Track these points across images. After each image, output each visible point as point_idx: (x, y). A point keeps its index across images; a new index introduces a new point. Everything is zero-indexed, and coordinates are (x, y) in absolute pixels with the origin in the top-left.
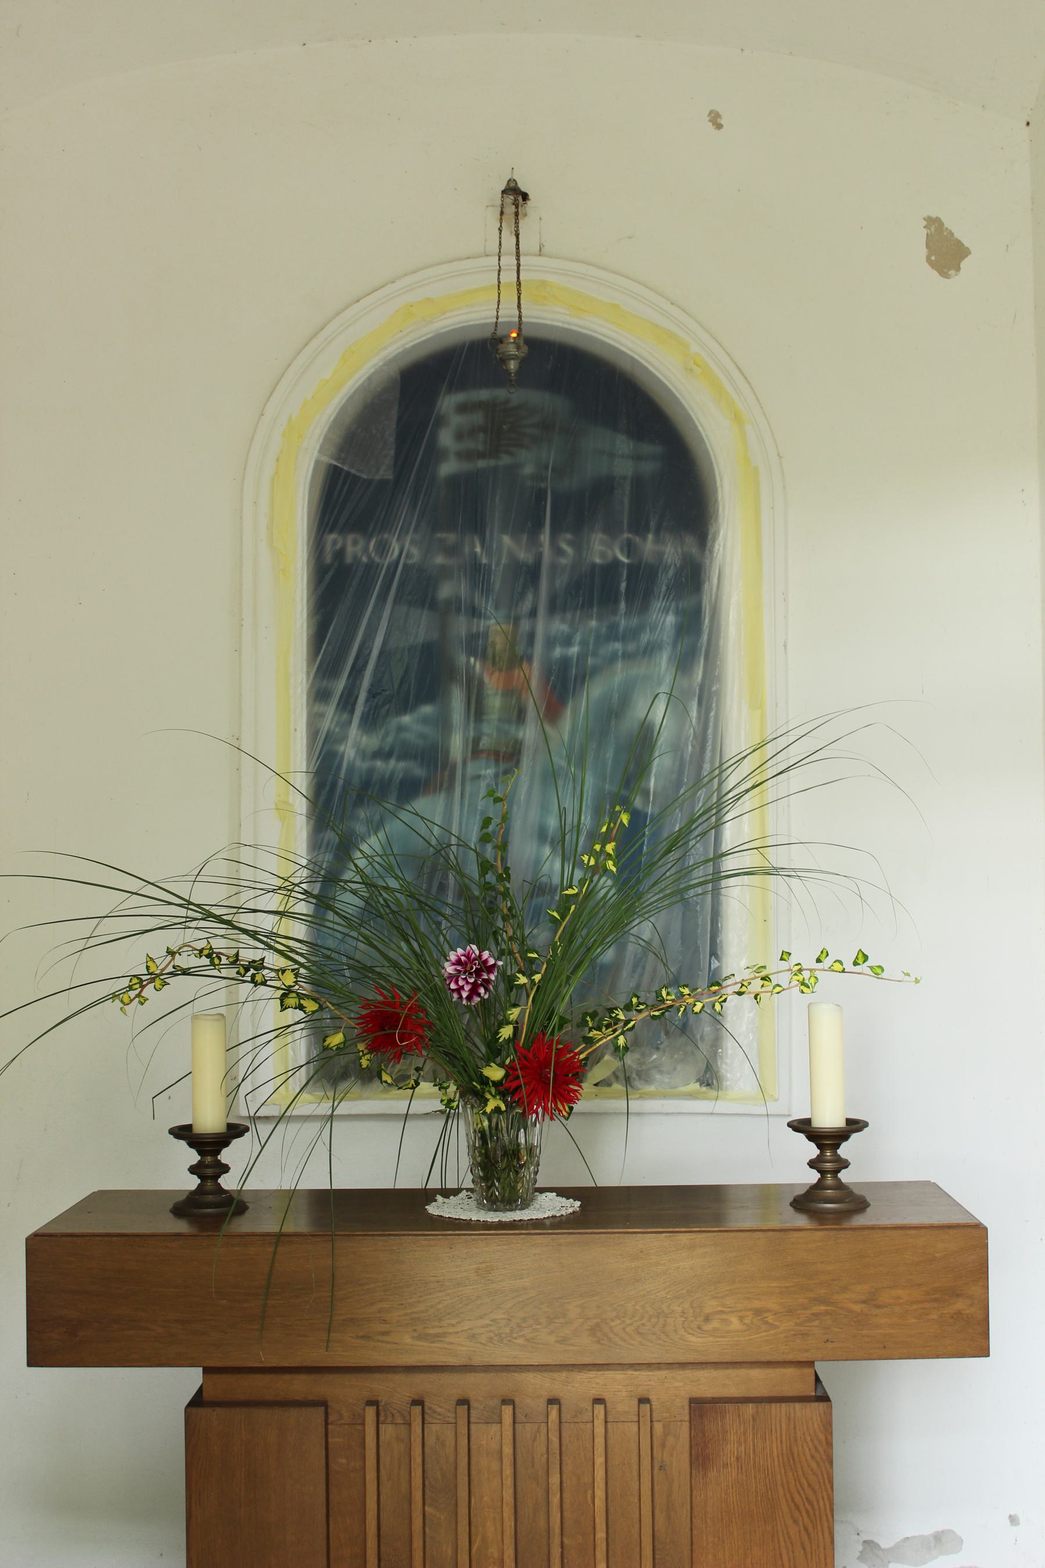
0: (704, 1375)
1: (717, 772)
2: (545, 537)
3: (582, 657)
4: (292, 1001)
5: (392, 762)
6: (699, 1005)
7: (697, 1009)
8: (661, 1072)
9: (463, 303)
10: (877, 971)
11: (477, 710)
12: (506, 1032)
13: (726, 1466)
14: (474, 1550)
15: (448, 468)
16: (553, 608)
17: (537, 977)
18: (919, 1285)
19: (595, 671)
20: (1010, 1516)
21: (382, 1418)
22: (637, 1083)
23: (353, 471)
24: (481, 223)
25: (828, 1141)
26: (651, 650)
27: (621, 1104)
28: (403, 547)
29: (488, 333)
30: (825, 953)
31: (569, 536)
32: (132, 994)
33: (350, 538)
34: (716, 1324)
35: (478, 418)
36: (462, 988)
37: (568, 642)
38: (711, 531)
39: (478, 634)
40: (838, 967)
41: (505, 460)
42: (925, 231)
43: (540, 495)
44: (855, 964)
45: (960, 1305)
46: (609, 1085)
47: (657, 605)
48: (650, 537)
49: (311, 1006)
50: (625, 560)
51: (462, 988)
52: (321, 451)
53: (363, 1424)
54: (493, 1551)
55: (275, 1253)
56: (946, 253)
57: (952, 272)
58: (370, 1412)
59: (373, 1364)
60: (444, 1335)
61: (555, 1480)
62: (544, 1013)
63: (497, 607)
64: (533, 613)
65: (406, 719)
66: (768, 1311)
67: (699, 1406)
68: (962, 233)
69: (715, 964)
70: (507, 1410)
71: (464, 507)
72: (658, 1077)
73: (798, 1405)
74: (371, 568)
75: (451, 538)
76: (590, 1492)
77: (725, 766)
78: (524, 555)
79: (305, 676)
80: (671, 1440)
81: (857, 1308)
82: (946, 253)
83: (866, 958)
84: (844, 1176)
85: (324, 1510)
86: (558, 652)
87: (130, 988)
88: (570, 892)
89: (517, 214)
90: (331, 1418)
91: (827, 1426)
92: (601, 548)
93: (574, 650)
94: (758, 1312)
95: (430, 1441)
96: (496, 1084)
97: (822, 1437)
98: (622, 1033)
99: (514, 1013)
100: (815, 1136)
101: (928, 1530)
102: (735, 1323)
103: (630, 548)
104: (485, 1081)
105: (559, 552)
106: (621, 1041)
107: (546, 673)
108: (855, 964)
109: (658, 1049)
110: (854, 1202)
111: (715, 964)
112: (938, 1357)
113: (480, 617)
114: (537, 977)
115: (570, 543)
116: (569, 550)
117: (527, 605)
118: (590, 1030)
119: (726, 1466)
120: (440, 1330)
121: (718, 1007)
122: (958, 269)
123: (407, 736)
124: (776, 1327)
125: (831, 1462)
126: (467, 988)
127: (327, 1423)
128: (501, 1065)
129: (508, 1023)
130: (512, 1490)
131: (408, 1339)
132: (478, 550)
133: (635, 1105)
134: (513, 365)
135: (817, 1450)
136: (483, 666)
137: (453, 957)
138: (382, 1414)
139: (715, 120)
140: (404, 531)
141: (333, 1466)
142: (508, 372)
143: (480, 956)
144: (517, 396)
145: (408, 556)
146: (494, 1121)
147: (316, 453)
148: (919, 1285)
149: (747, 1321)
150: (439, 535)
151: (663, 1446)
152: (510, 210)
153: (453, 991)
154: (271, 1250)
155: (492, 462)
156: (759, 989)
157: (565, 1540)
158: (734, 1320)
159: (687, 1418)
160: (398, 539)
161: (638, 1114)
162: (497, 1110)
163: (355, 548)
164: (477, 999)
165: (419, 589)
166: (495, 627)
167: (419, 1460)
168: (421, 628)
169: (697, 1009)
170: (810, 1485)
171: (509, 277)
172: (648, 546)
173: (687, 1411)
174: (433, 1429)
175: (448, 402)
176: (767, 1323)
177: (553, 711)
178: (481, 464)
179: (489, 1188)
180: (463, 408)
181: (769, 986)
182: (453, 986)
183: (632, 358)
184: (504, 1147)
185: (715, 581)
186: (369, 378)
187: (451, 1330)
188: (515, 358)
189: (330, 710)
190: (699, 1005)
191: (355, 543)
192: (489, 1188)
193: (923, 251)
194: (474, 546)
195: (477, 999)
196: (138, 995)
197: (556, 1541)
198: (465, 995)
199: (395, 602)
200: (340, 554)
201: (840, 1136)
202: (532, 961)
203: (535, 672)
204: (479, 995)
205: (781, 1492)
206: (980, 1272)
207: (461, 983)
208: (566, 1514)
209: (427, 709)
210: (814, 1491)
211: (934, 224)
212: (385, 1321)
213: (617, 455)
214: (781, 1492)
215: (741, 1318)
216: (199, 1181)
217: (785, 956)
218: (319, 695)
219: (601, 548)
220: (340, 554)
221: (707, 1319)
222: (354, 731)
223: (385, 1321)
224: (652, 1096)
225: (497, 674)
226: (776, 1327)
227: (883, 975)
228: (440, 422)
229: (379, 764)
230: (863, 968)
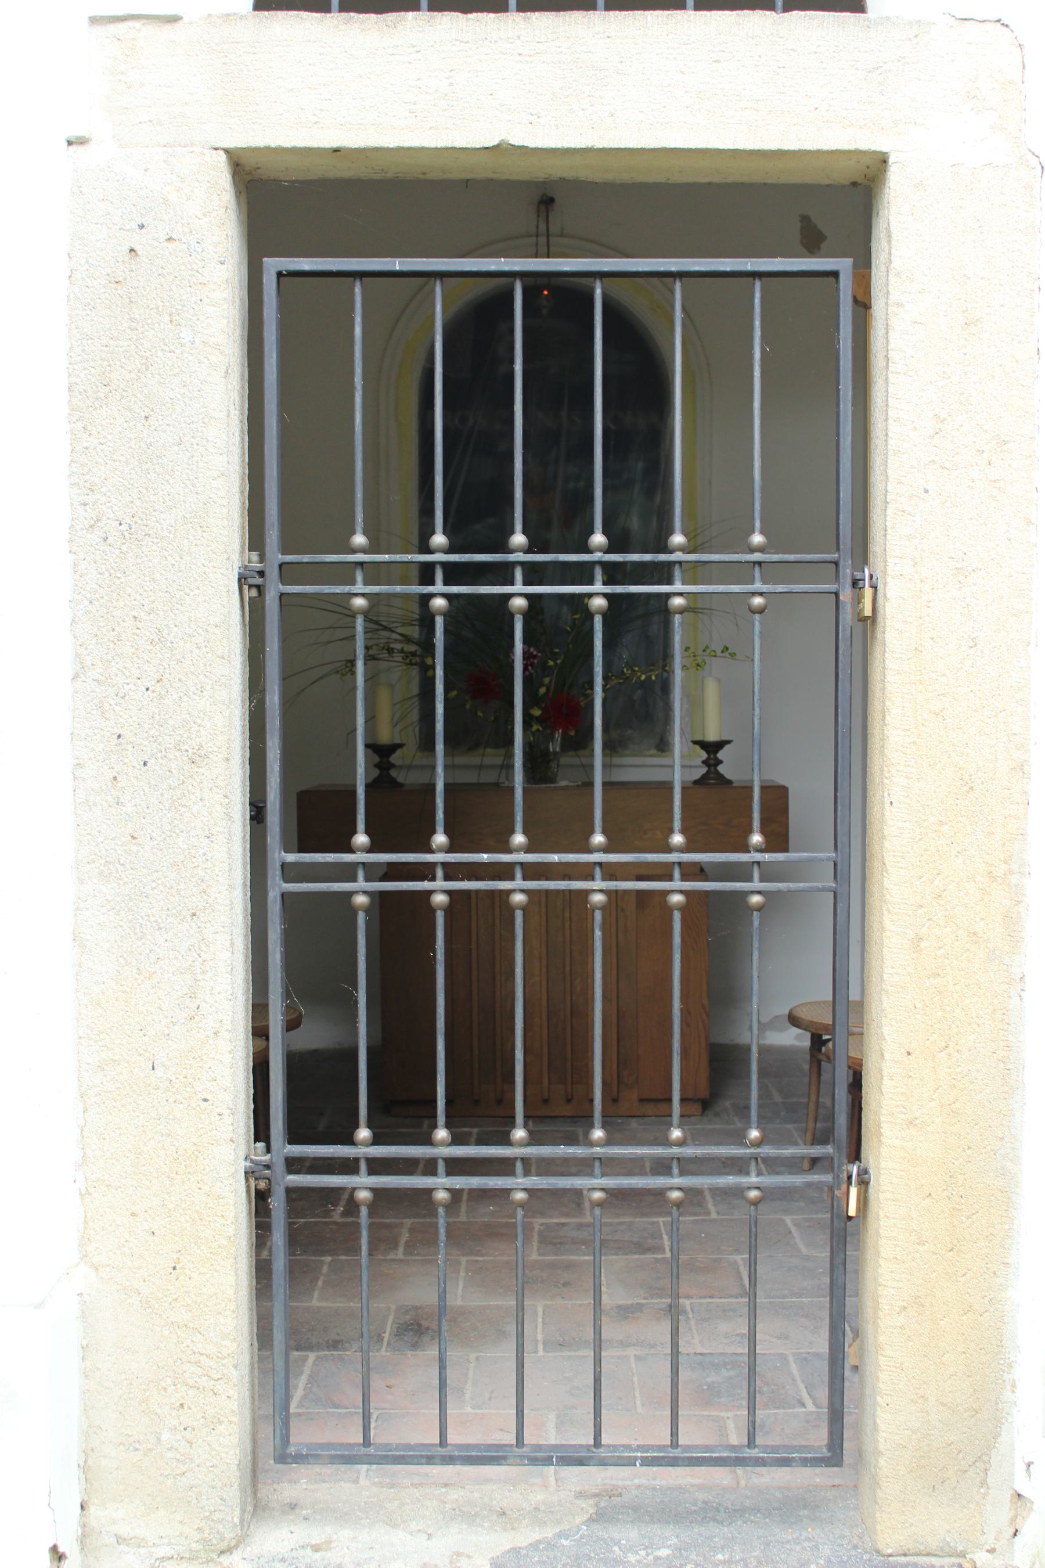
10: (733, 655)
17: (559, 661)
25: (712, 748)
30: (707, 647)
61: (567, 915)
65: (478, 527)
83: (727, 649)
84: (720, 768)
86: (571, 485)
96: (537, 718)
99: (547, 680)
110: (724, 782)
114: (559, 661)
122: (819, 249)
128: (540, 708)
134: (545, 311)
158: (659, 833)
162: (538, 730)
201: (720, 745)
202: (556, 653)
211: (806, 220)
230: (726, 654)
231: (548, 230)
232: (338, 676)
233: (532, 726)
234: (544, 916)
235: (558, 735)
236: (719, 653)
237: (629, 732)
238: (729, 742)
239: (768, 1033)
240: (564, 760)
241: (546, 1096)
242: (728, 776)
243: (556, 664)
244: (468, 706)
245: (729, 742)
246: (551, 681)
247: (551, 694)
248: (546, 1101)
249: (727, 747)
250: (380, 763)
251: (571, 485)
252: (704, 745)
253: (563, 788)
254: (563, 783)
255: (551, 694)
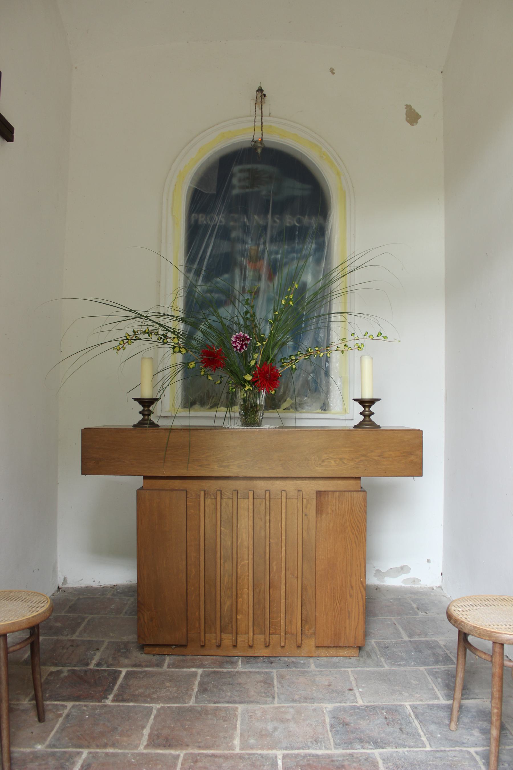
0: (322, 482)
1: (329, 295)
2: (269, 216)
3: (282, 259)
4: (177, 349)
5: (213, 294)
6: (322, 354)
7: (321, 355)
8: (307, 406)
9: (240, 132)
11: (244, 278)
12: (253, 363)
13: (329, 513)
14: (238, 543)
15: (235, 192)
16: (272, 241)
17: (264, 343)
18: (399, 450)
19: (286, 264)
20: (428, 560)
21: (206, 496)
22: (299, 409)
23: (202, 190)
24: (248, 104)
25: (367, 404)
26: (306, 257)
27: (293, 415)
28: (219, 219)
29: (249, 145)
31: (277, 216)
32: (121, 346)
33: (200, 215)
34: (326, 463)
35: (246, 175)
36: (238, 346)
37: (277, 253)
38: (329, 213)
39: (245, 250)
40: (371, 337)
41: (256, 189)
42: (405, 110)
43: (268, 201)
44: (378, 336)
45: (412, 458)
46: (289, 410)
47: (308, 240)
48: (306, 217)
49: (183, 351)
50: (298, 225)
51: (238, 346)
52: (191, 183)
53: (200, 498)
54: (245, 544)
55: (169, 435)
56: (413, 117)
57: (414, 124)
58: (202, 493)
59: (203, 476)
60: (229, 465)
61: (268, 518)
62: (266, 358)
63: (252, 241)
64: (264, 243)
65: (218, 280)
66: (345, 459)
67: (319, 494)
68: (418, 110)
69: (327, 365)
70: (251, 494)
71: (241, 205)
72: (306, 407)
73: (354, 493)
74: (207, 227)
75: (236, 216)
76: (280, 524)
77: (332, 294)
78: (261, 223)
79: (183, 261)
80: (309, 505)
81: (376, 458)
82: (413, 117)
83: (381, 334)
84: (372, 417)
85: (185, 527)
86: (273, 257)
87: (120, 344)
88: (277, 313)
89: (262, 102)
90: (188, 496)
91: (365, 500)
92: (289, 220)
93: (279, 256)
94: (341, 459)
95: (224, 504)
96: (249, 382)
97: (363, 504)
98: (294, 364)
99: (256, 356)
100: (362, 402)
101: (398, 565)
102: (333, 463)
103: (299, 221)
104: (245, 381)
105: (274, 222)
106: (294, 367)
107: (269, 265)
108: (378, 336)
109: (306, 396)
111: (327, 365)
112: (405, 476)
113: (246, 244)
114: (264, 343)
115: (278, 218)
116: (278, 221)
117: (262, 241)
118: (283, 363)
119: (329, 513)
120: (228, 464)
121: (328, 355)
122: (417, 123)
123: (218, 285)
124: (348, 464)
125: (366, 513)
126: (239, 346)
127: (187, 498)
129: (253, 359)
130: (252, 521)
131: (216, 467)
132: (246, 220)
133: (298, 415)
135: (361, 509)
136: (246, 261)
137: (234, 336)
138: (206, 495)
139: (332, 71)
140: (218, 214)
141: (189, 513)
142: (257, 153)
143: (244, 335)
144: (259, 167)
145: (221, 222)
146: (248, 393)
147: (189, 184)
148: (399, 450)
149: (337, 462)
150: (232, 215)
151: (306, 507)
152: (259, 100)
153: (234, 347)
154: (168, 434)
155: (251, 190)
156: (343, 349)
157: (271, 540)
158: (333, 462)
159: (315, 498)
160: (217, 215)
161: (299, 418)
162: (249, 389)
163: (202, 219)
164: (243, 350)
165: (224, 233)
166: (250, 246)
167: (219, 510)
168: (225, 247)
169: (321, 355)
170: (358, 521)
171: (259, 124)
172: (306, 220)
173: (315, 495)
174: (224, 500)
175: (236, 169)
176: (344, 463)
177: (271, 278)
178: (247, 190)
179: (246, 418)
180: (241, 171)
181: (347, 348)
182: (234, 345)
183: (302, 153)
184: (251, 404)
185: (330, 231)
186: (208, 158)
187: (231, 464)
188: (260, 147)
189: (191, 275)
190: (322, 354)
191: (202, 217)
192: (246, 418)
193: (405, 116)
194: (244, 219)
195: (243, 350)
196: (123, 347)
197: (268, 539)
198: (238, 348)
199: (215, 238)
200: (196, 221)
201: (372, 402)
203: (265, 262)
204: (243, 349)
205: (348, 523)
206: (420, 446)
207: (237, 344)
208: (271, 531)
209: (226, 276)
210: (360, 523)
211: (409, 107)
212: (208, 460)
213: (294, 188)
214: (348, 523)
215: (335, 461)
216: (142, 417)
217: (353, 334)
218: (188, 270)
219: (289, 220)
220: (196, 221)
221: (323, 461)
222: (200, 282)
223: (208, 460)
224: (304, 413)
225: (251, 263)
226: (348, 464)
227: (388, 340)
228: (232, 176)
229: (208, 295)
230: (381, 337)
231: (262, 114)
232: (115, 351)
233: (245, 386)
234: (251, 518)
235: (263, 393)
236: (375, 337)
237: (306, 398)
238: (378, 400)
239: (386, 579)
240: (267, 414)
241: (251, 643)
242: (377, 423)
243: (262, 344)
244: (202, 373)
245: (378, 400)
246: (258, 356)
247: (258, 365)
248: (251, 647)
249: (377, 403)
250: (143, 410)
251: (273, 257)
252: (362, 402)
253: (265, 429)
254: (266, 426)
255: (258, 365)
